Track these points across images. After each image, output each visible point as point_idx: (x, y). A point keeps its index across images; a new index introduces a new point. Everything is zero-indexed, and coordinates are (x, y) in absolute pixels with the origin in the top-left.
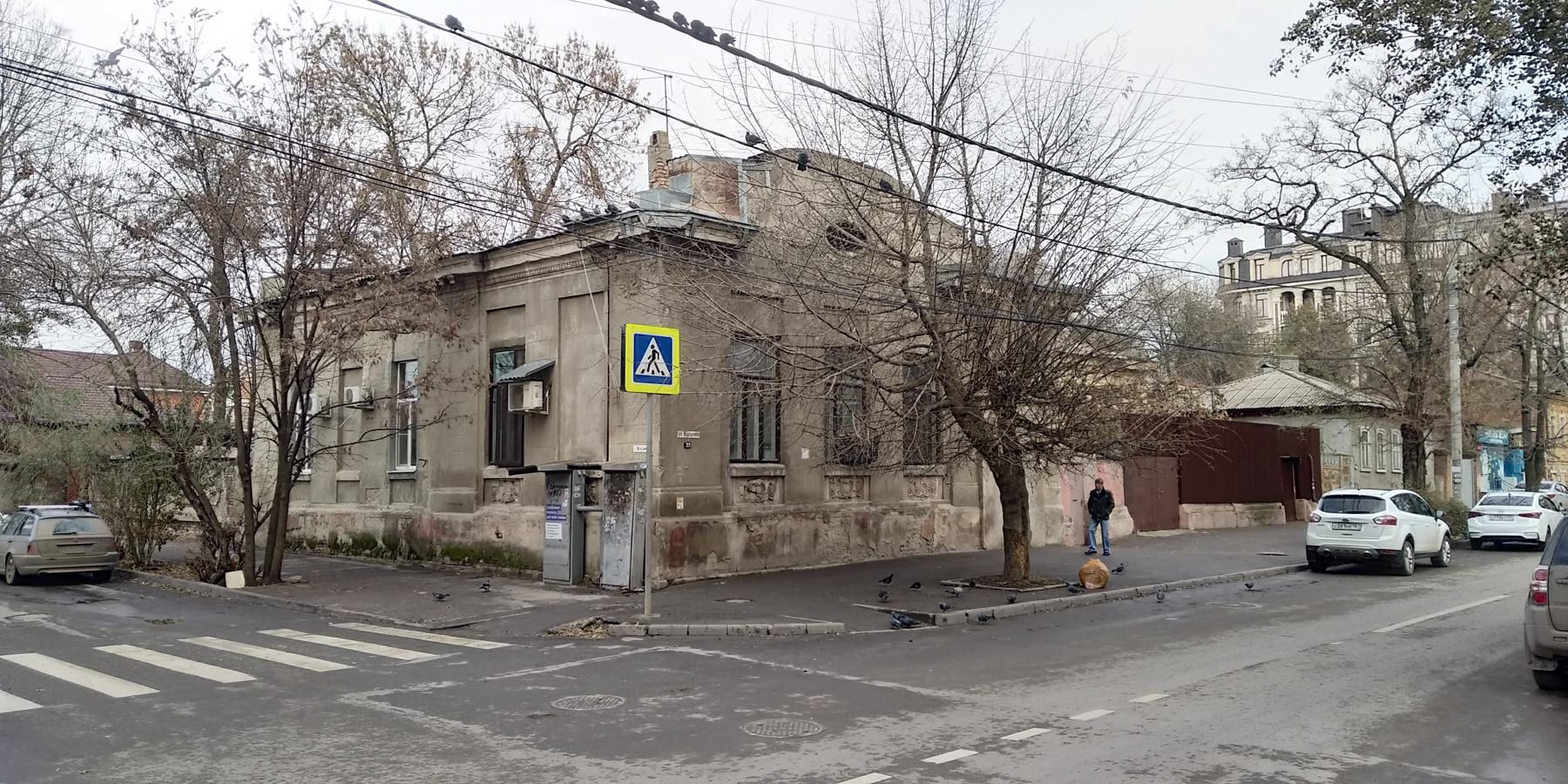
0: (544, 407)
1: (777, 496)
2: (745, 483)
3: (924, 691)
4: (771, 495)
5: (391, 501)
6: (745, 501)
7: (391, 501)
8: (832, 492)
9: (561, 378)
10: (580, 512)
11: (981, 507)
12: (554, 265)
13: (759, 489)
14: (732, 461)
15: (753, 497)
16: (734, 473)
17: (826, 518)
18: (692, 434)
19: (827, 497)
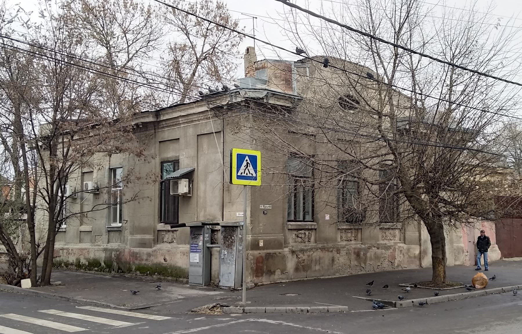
1: (312, 239)
2: (295, 232)
5: (108, 242)
6: (295, 242)
7: (108, 242)
8: (341, 237)
9: (199, 176)
10: (208, 248)
11: (420, 245)
13: (303, 236)
14: (289, 221)
15: (300, 240)
16: (290, 227)
18: (268, 207)
19: (339, 240)
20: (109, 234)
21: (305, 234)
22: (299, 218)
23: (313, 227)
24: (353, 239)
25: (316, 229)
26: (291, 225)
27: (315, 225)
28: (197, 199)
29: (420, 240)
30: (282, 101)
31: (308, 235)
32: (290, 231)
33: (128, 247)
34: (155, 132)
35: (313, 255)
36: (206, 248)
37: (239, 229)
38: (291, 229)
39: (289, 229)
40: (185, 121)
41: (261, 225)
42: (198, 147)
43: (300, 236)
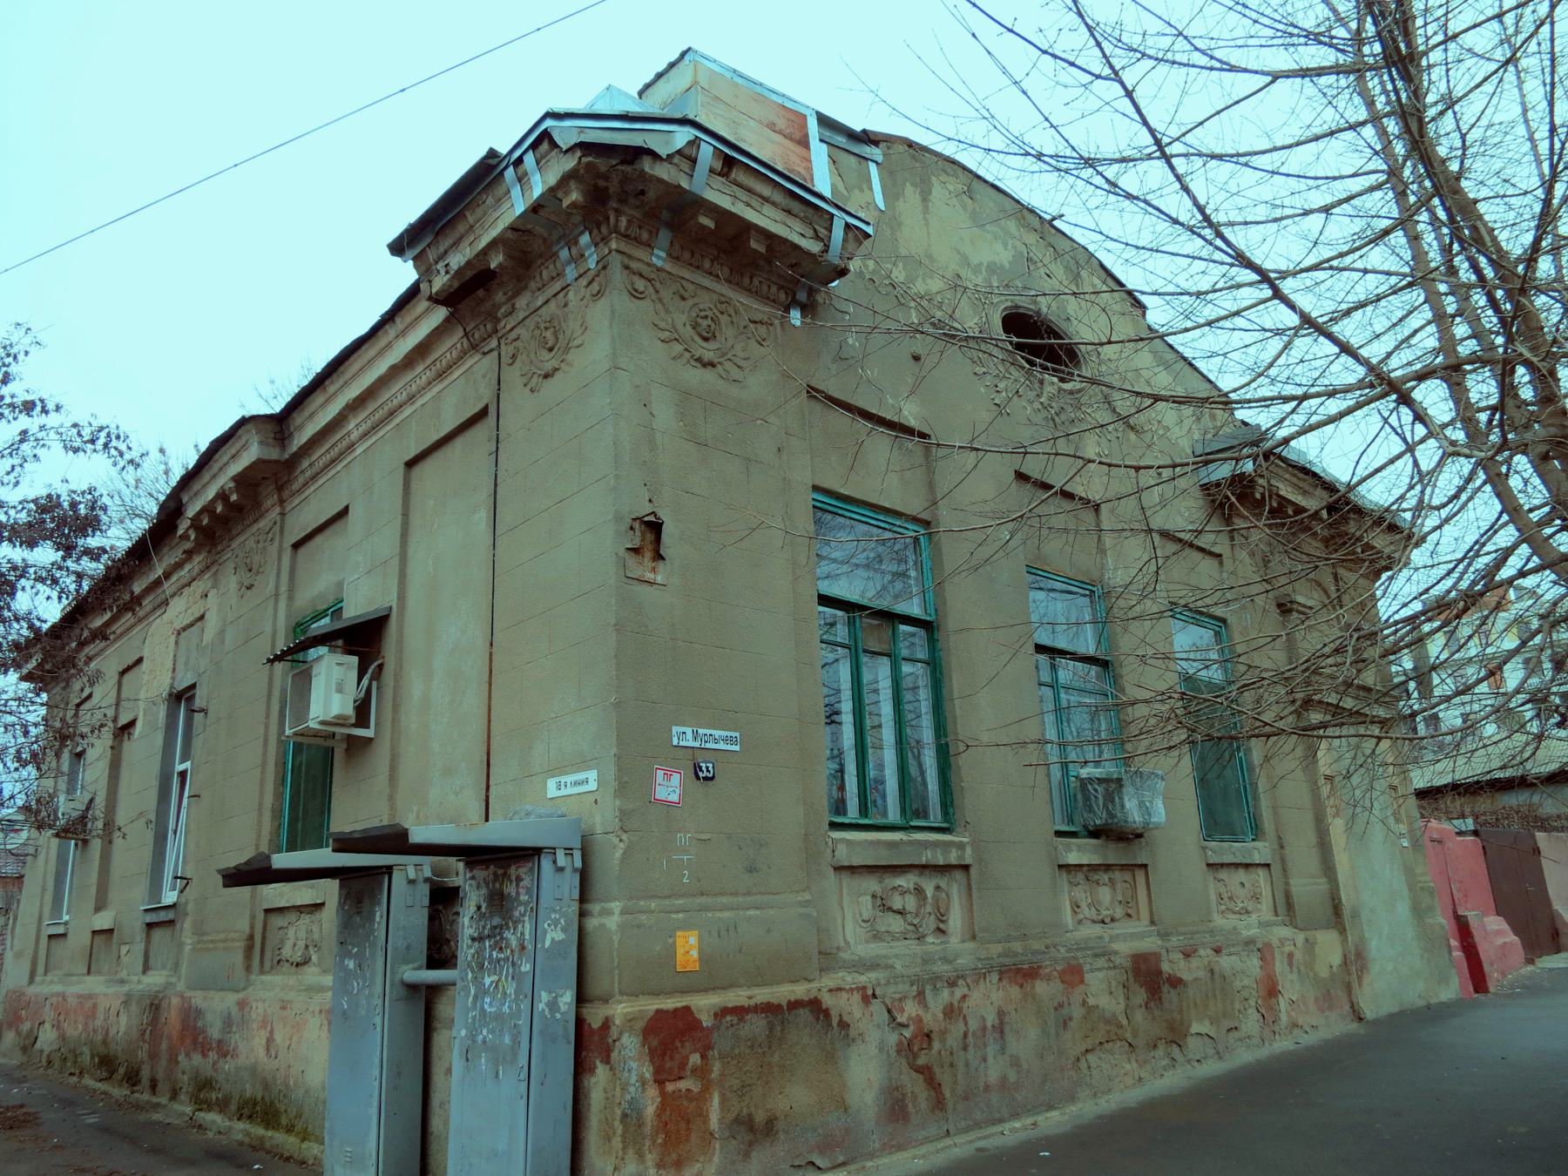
0: (362, 712)
1: (956, 920)
2: (872, 884)
3: (1054, 1121)
4: (941, 917)
5: (146, 968)
6: (877, 937)
7: (146, 968)
8: (1076, 906)
9: (407, 645)
10: (413, 988)
11: (1342, 931)
12: (395, 393)
13: (911, 903)
14: (834, 826)
15: (896, 924)
16: (844, 856)
17: (1073, 974)
18: (719, 739)
19: (1068, 918)
20: (148, 935)
21: (919, 891)
22: (885, 814)
23: (953, 858)
24: (1119, 912)
25: (966, 868)
26: (849, 843)
27: (961, 846)
28: (393, 748)
29: (1337, 908)
30: (768, 209)
31: (936, 900)
32: (846, 880)
33: (181, 986)
34: (283, 514)
35: (970, 1002)
36: (403, 991)
37: (546, 863)
38: (852, 869)
39: (839, 869)
40: (364, 427)
41: (682, 839)
42: (406, 515)
43: (897, 905)
